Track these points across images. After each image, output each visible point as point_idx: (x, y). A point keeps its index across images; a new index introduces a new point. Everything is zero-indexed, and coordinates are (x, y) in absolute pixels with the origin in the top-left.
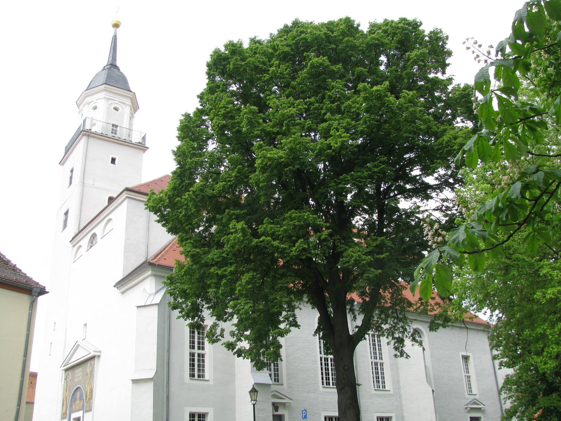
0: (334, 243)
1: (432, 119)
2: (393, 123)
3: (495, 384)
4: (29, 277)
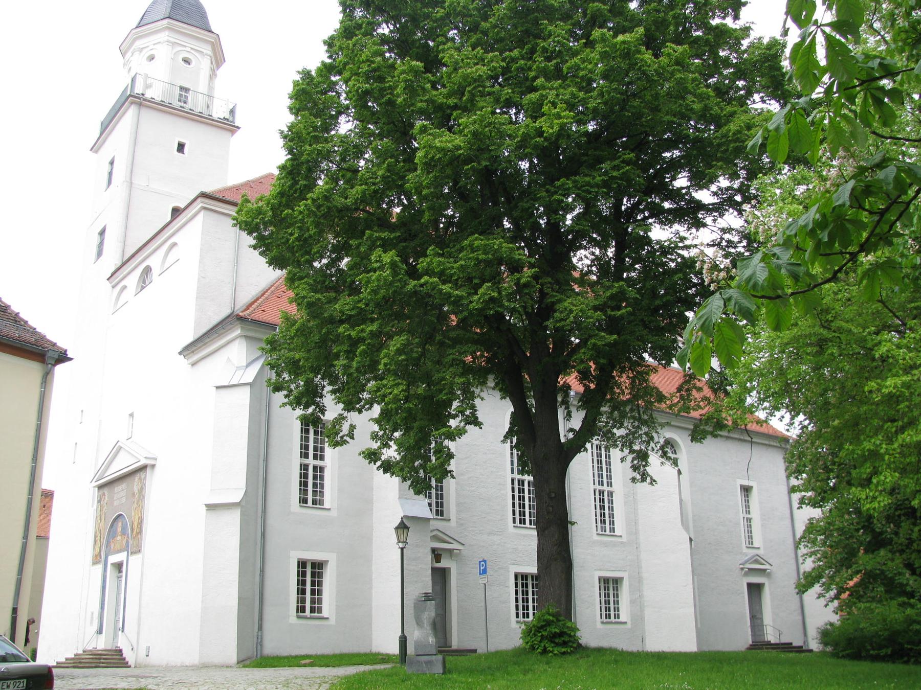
0: (541, 291)
1: (712, 94)
2: (648, 97)
3: (791, 533)
4: (40, 334)
